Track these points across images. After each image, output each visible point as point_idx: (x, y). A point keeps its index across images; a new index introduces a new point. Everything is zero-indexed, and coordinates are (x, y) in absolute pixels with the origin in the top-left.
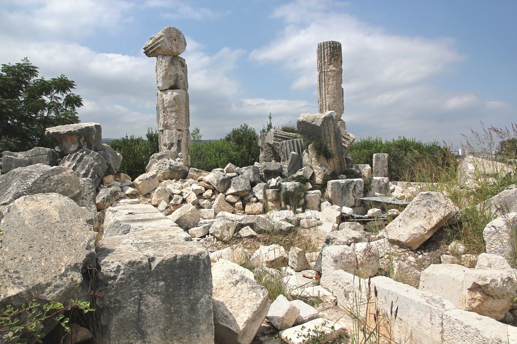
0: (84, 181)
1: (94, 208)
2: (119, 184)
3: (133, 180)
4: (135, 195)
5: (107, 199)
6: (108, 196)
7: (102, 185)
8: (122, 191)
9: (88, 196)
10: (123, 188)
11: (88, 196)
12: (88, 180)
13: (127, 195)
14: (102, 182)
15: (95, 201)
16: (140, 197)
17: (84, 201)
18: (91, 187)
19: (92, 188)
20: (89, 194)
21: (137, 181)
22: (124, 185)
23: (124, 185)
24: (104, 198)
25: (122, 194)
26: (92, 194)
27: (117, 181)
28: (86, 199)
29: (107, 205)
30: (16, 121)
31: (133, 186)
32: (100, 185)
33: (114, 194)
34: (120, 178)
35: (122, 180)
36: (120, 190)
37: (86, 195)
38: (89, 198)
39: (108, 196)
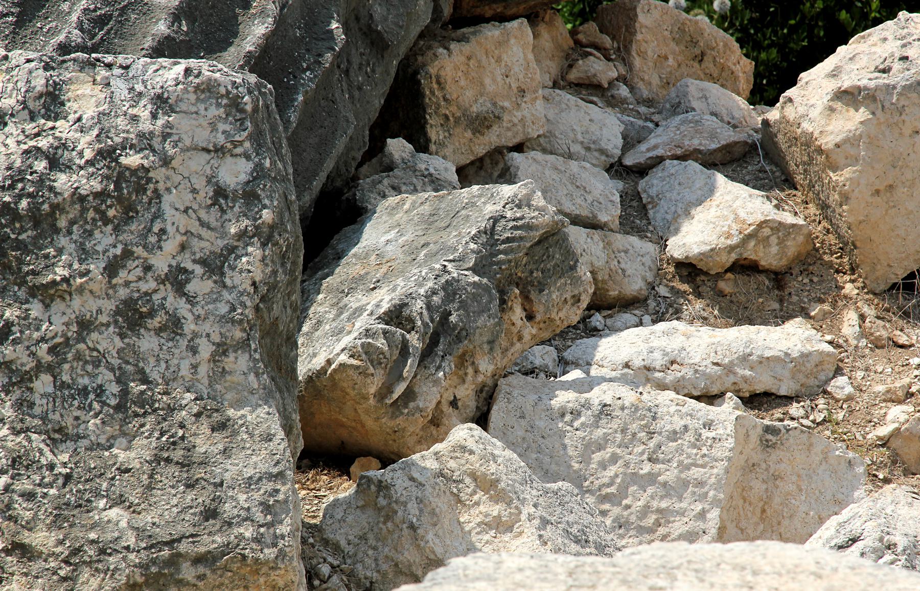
0: (161, 102)
1: (260, 440)
2: (607, 127)
3: (770, 85)
4: (779, 278)
5: (435, 333)
6: (451, 289)
7: (398, 147)
8: (638, 216)
9: (199, 286)
10: (651, 185)
11: (199, 286)
12: (208, 90)
13: (689, 270)
14: (406, 111)
15: (278, 350)
16: (838, 300)
17: (148, 343)
18: (235, 172)
19: (250, 196)
20: (216, 265)
21: (811, 101)
22: (658, 141)
23: (658, 141)
24: (396, 316)
25: (633, 263)
26: (252, 262)
27: (589, 89)
28: (174, 326)
29: (429, 397)
30: (752, 31)
31: (760, 160)
32: (376, 148)
33: (521, 268)
34: (622, 52)
35: (649, 77)
36: (610, 214)
37: (177, 279)
38: (207, 313)
39: (451, 289)
